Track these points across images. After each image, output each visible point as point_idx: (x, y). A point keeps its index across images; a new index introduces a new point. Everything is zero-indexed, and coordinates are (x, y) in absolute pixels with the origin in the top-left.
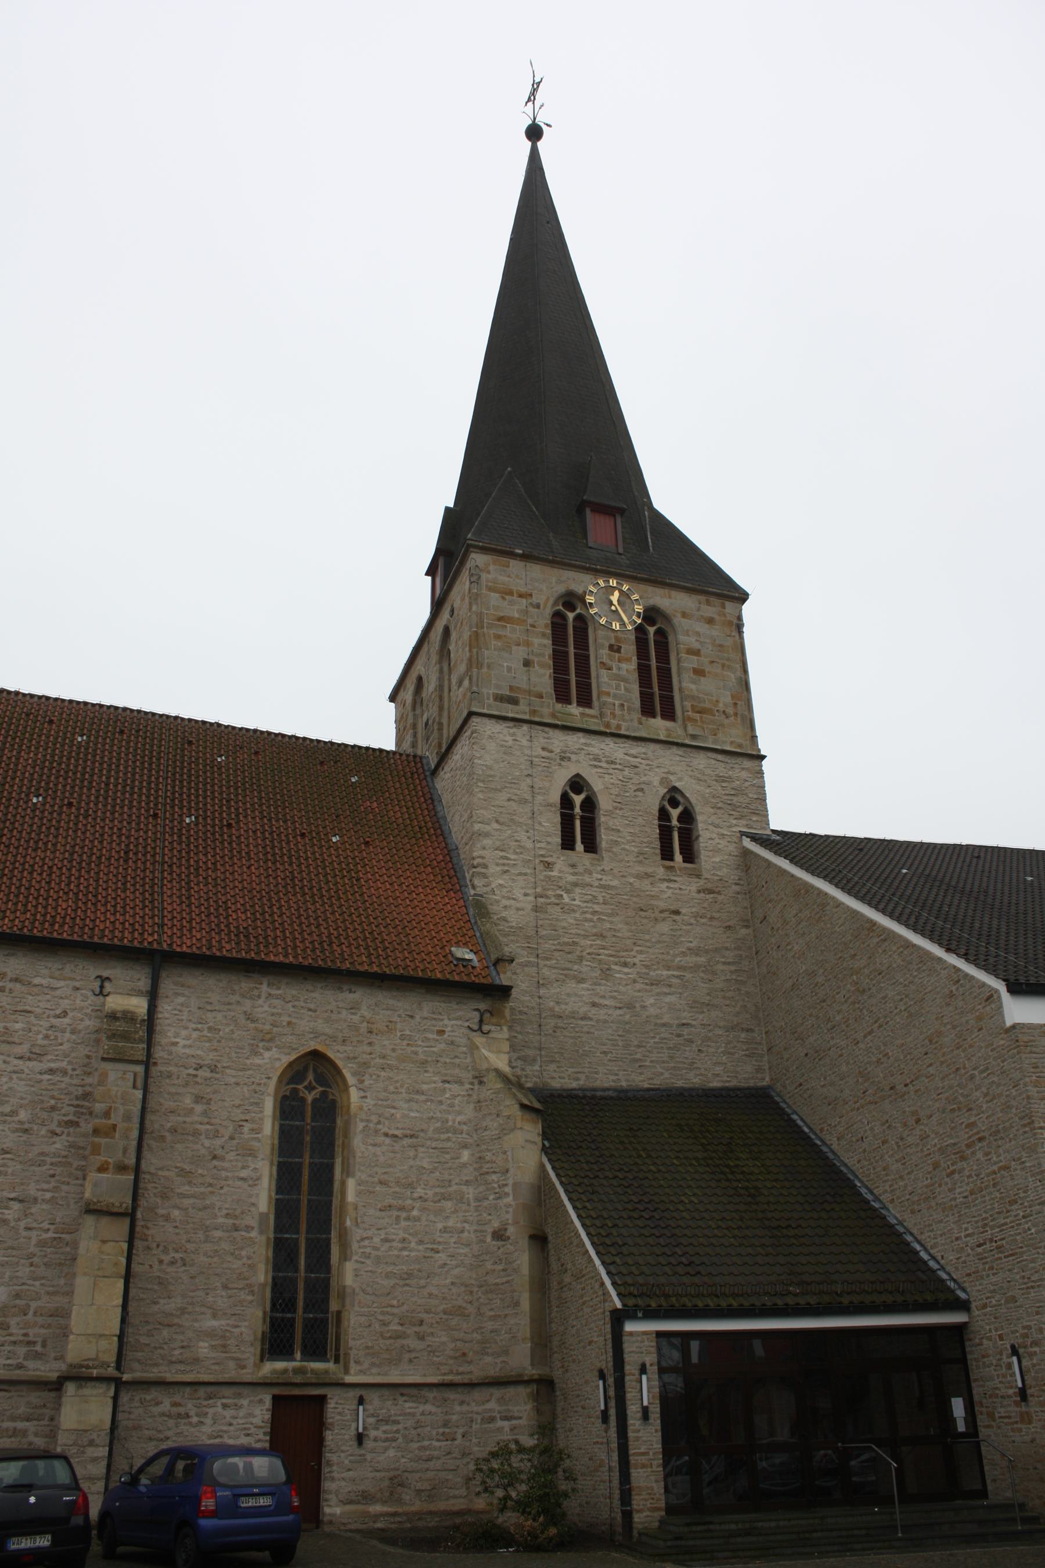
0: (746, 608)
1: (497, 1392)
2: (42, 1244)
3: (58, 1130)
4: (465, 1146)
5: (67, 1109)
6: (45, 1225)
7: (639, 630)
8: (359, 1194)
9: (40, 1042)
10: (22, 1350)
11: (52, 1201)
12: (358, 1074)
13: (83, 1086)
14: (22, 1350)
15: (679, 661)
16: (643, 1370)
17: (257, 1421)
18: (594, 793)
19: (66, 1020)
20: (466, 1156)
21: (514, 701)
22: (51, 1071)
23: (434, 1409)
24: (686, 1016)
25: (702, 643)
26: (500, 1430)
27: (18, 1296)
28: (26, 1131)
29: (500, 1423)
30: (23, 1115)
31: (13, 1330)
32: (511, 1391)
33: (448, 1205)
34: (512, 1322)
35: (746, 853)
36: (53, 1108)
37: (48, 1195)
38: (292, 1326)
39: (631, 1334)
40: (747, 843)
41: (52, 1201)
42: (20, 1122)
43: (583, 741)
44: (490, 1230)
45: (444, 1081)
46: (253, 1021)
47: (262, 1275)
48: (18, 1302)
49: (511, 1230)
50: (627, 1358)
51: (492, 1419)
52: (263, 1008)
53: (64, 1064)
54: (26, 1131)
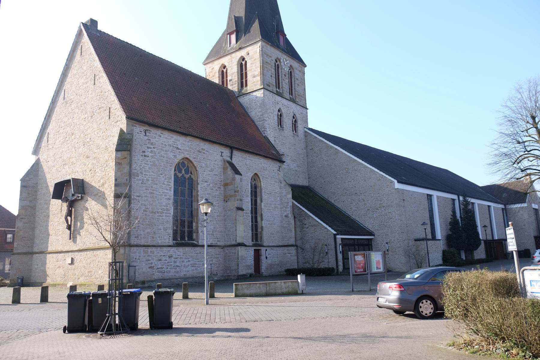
0: (306, 69)
1: (286, 248)
2: (217, 216)
3: (217, 189)
4: (278, 197)
5: (218, 184)
6: (217, 212)
7: (288, 71)
8: (264, 206)
9: (212, 167)
10: (216, 240)
11: (218, 206)
12: (263, 179)
13: (221, 179)
14: (216, 240)
15: (295, 81)
16: (340, 245)
17: (252, 254)
18: (282, 113)
19: (216, 162)
20: (278, 198)
21: (269, 86)
22: (215, 175)
23: (275, 252)
24: (297, 168)
25: (299, 77)
26: (288, 256)
27: (215, 228)
28: (212, 189)
29: (288, 255)
30: (211, 185)
31: (215, 235)
32: (290, 248)
33: (276, 209)
34: (290, 234)
35: (306, 132)
36: (216, 184)
37: (217, 205)
38: (185, 231)
39: (338, 238)
40: (306, 129)
41: (218, 206)
42: (211, 187)
43: (281, 99)
44: (284, 215)
45: (275, 182)
46: (247, 165)
47: (430, 231)
48: (215, 229)
49: (290, 215)
50: (337, 242)
51: (286, 254)
52: (248, 162)
53: (217, 173)
54: (212, 189)
